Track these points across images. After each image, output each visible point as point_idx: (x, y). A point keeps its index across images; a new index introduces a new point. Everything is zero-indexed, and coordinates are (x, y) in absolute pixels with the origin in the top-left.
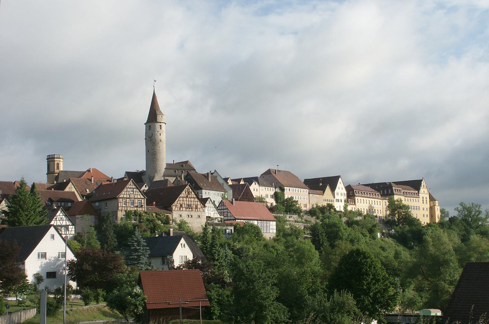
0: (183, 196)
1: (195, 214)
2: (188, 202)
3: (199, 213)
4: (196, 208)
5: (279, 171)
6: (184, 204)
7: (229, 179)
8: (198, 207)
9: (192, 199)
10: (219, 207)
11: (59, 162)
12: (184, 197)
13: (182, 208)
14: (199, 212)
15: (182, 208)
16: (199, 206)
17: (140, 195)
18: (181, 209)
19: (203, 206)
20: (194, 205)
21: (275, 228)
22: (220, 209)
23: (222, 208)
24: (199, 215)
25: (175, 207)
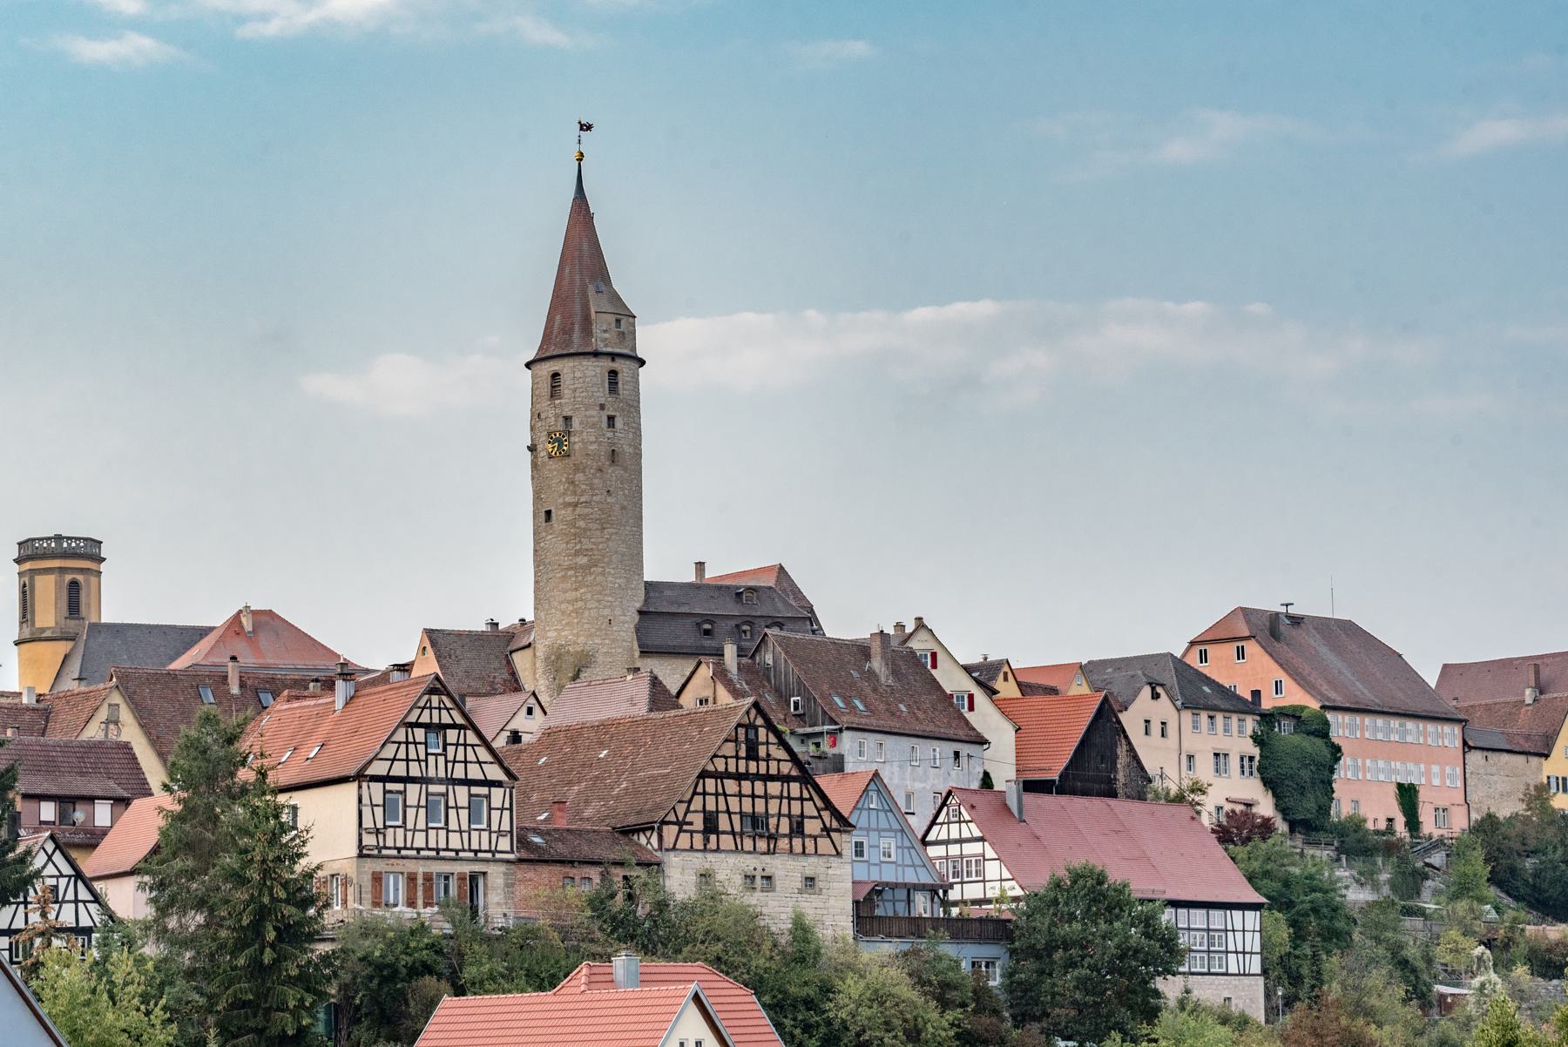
0: (721, 768)
1: (786, 868)
2: (747, 802)
3: (811, 865)
4: (798, 829)
5: (1296, 621)
6: (728, 811)
7: (1006, 669)
9: (774, 788)
11: (80, 578)
12: (727, 775)
13: (713, 838)
14: (814, 860)
15: (713, 838)
17: (479, 763)
18: (712, 845)
19: (835, 824)
20: (785, 822)
21: (1257, 948)
22: (943, 836)
24: (809, 873)
25: (676, 828)
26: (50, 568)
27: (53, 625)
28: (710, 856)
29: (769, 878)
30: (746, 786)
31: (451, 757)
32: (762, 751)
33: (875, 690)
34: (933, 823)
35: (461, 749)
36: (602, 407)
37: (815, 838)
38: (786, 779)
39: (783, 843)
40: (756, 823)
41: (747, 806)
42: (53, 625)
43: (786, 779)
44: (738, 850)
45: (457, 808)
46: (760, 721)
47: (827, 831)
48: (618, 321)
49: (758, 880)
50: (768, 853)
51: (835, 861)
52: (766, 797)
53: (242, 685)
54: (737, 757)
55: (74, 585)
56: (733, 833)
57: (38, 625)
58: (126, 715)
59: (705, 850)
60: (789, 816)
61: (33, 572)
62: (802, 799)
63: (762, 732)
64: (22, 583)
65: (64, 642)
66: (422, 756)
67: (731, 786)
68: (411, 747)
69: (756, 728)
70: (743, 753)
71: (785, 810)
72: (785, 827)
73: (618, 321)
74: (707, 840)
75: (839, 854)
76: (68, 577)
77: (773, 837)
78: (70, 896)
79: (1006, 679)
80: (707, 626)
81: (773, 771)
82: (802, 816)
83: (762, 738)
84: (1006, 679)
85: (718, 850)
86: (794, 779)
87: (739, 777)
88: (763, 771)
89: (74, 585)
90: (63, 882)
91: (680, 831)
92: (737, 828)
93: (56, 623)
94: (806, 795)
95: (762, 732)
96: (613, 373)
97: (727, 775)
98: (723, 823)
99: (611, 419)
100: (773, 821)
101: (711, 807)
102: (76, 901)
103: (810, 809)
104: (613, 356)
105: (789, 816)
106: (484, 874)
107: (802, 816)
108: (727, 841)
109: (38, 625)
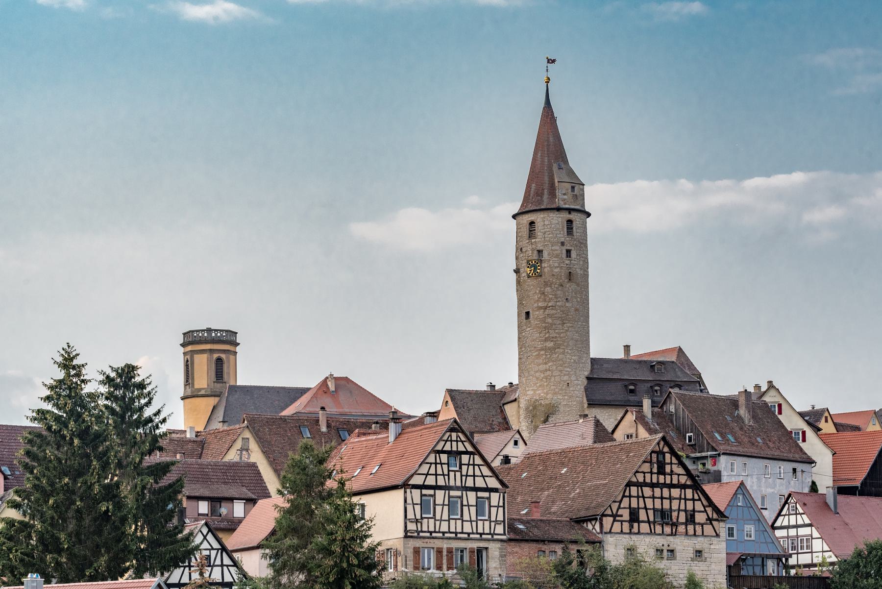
0: (641, 480)
2: (658, 503)
3: (700, 543)
4: (691, 519)
6: (646, 508)
7: (826, 414)
8: (697, 521)
9: (676, 492)
10: (781, 518)
11: (223, 356)
12: (644, 484)
13: (636, 525)
14: (701, 539)
15: (636, 525)
16: (700, 518)
17: (483, 476)
18: (635, 530)
20: (683, 514)
22: (785, 523)
23: (793, 523)
24: (698, 548)
25: (611, 519)
26: (204, 350)
27: (206, 387)
28: (634, 537)
29: (672, 551)
30: (657, 492)
31: (464, 473)
32: (668, 469)
33: (741, 429)
34: (779, 515)
35: (471, 467)
36: (563, 244)
37: (702, 525)
38: (684, 487)
39: (681, 529)
40: (664, 516)
41: (658, 505)
42: (206, 387)
43: (684, 487)
44: (652, 533)
45: (468, 506)
46: (666, 449)
47: (710, 520)
48: (573, 188)
49: (665, 552)
50: (672, 535)
51: (715, 540)
52: (670, 498)
53: (329, 426)
54: (651, 473)
55: (219, 361)
56: (649, 522)
57: (196, 386)
58: (253, 445)
59: (630, 533)
60: (685, 511)
61: (193, 352)
62: (693, 500)
63: (668, 456)
64: (186, 359)
65: (213, 398)
66: (446, 472)
67: (647, 491)
68: (439, 466)
69: (664, 454)
70: (655, 470)
71: (683, 507)
72: (682, 518)
73: (573, 188)
74: (631, 527)
75: (717, 535)
76: (216, 356)
77: (675, 525)
78: (218, 562)
79: (826, 421)
80: (632, 387)
81: (675, 482)
82: (694, 510)
83: (668, 460)
84: (826, 421)
85: (639, 533)
86: (688, 487)
87: (652, 486)
88: (668, 481)
89: (219, 361)
90: (213, 553)
91: (614, 521)
92: (651, 519)
93: (208, 385)
94: (696, 497)
95: (668, 456)
96: (570, 222)
97: (644, 484)
98: (642, 516)
99: (568, 252)
100: (675, 514)
101: (634, 505)
102: (222, 565)
103: (699, 506)
104: (570, 211)
105: (685, 511)
106: (487, 548)
107: (694, 510)
108: (645, 527)
109: (196, 386)
